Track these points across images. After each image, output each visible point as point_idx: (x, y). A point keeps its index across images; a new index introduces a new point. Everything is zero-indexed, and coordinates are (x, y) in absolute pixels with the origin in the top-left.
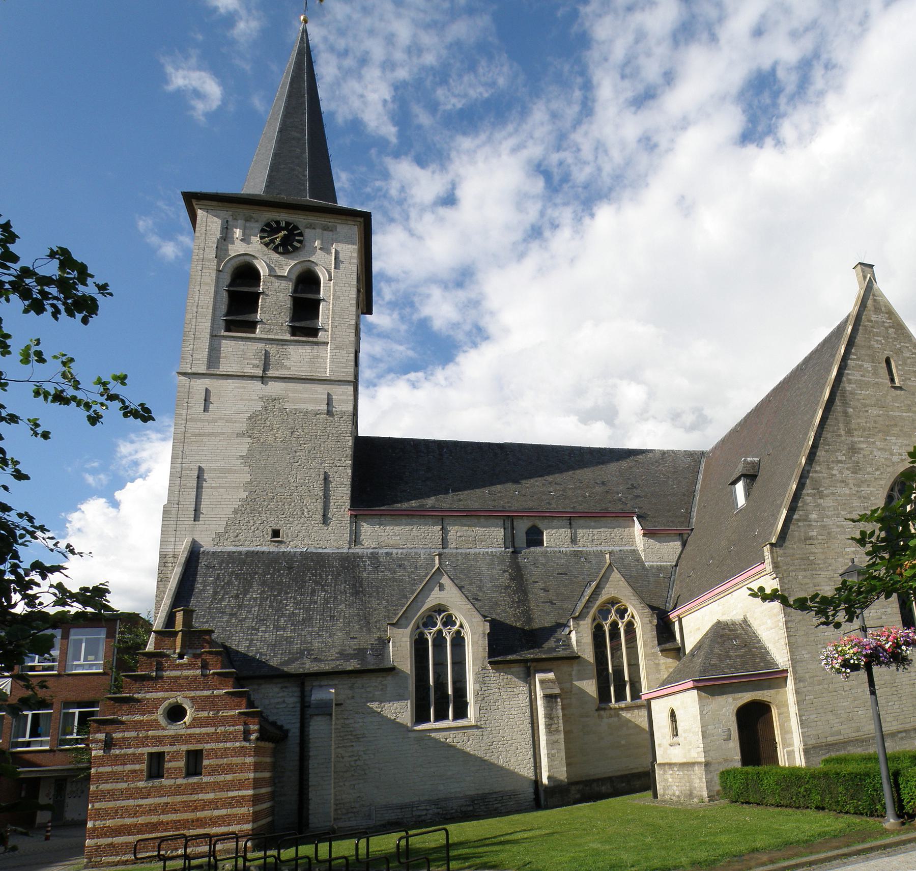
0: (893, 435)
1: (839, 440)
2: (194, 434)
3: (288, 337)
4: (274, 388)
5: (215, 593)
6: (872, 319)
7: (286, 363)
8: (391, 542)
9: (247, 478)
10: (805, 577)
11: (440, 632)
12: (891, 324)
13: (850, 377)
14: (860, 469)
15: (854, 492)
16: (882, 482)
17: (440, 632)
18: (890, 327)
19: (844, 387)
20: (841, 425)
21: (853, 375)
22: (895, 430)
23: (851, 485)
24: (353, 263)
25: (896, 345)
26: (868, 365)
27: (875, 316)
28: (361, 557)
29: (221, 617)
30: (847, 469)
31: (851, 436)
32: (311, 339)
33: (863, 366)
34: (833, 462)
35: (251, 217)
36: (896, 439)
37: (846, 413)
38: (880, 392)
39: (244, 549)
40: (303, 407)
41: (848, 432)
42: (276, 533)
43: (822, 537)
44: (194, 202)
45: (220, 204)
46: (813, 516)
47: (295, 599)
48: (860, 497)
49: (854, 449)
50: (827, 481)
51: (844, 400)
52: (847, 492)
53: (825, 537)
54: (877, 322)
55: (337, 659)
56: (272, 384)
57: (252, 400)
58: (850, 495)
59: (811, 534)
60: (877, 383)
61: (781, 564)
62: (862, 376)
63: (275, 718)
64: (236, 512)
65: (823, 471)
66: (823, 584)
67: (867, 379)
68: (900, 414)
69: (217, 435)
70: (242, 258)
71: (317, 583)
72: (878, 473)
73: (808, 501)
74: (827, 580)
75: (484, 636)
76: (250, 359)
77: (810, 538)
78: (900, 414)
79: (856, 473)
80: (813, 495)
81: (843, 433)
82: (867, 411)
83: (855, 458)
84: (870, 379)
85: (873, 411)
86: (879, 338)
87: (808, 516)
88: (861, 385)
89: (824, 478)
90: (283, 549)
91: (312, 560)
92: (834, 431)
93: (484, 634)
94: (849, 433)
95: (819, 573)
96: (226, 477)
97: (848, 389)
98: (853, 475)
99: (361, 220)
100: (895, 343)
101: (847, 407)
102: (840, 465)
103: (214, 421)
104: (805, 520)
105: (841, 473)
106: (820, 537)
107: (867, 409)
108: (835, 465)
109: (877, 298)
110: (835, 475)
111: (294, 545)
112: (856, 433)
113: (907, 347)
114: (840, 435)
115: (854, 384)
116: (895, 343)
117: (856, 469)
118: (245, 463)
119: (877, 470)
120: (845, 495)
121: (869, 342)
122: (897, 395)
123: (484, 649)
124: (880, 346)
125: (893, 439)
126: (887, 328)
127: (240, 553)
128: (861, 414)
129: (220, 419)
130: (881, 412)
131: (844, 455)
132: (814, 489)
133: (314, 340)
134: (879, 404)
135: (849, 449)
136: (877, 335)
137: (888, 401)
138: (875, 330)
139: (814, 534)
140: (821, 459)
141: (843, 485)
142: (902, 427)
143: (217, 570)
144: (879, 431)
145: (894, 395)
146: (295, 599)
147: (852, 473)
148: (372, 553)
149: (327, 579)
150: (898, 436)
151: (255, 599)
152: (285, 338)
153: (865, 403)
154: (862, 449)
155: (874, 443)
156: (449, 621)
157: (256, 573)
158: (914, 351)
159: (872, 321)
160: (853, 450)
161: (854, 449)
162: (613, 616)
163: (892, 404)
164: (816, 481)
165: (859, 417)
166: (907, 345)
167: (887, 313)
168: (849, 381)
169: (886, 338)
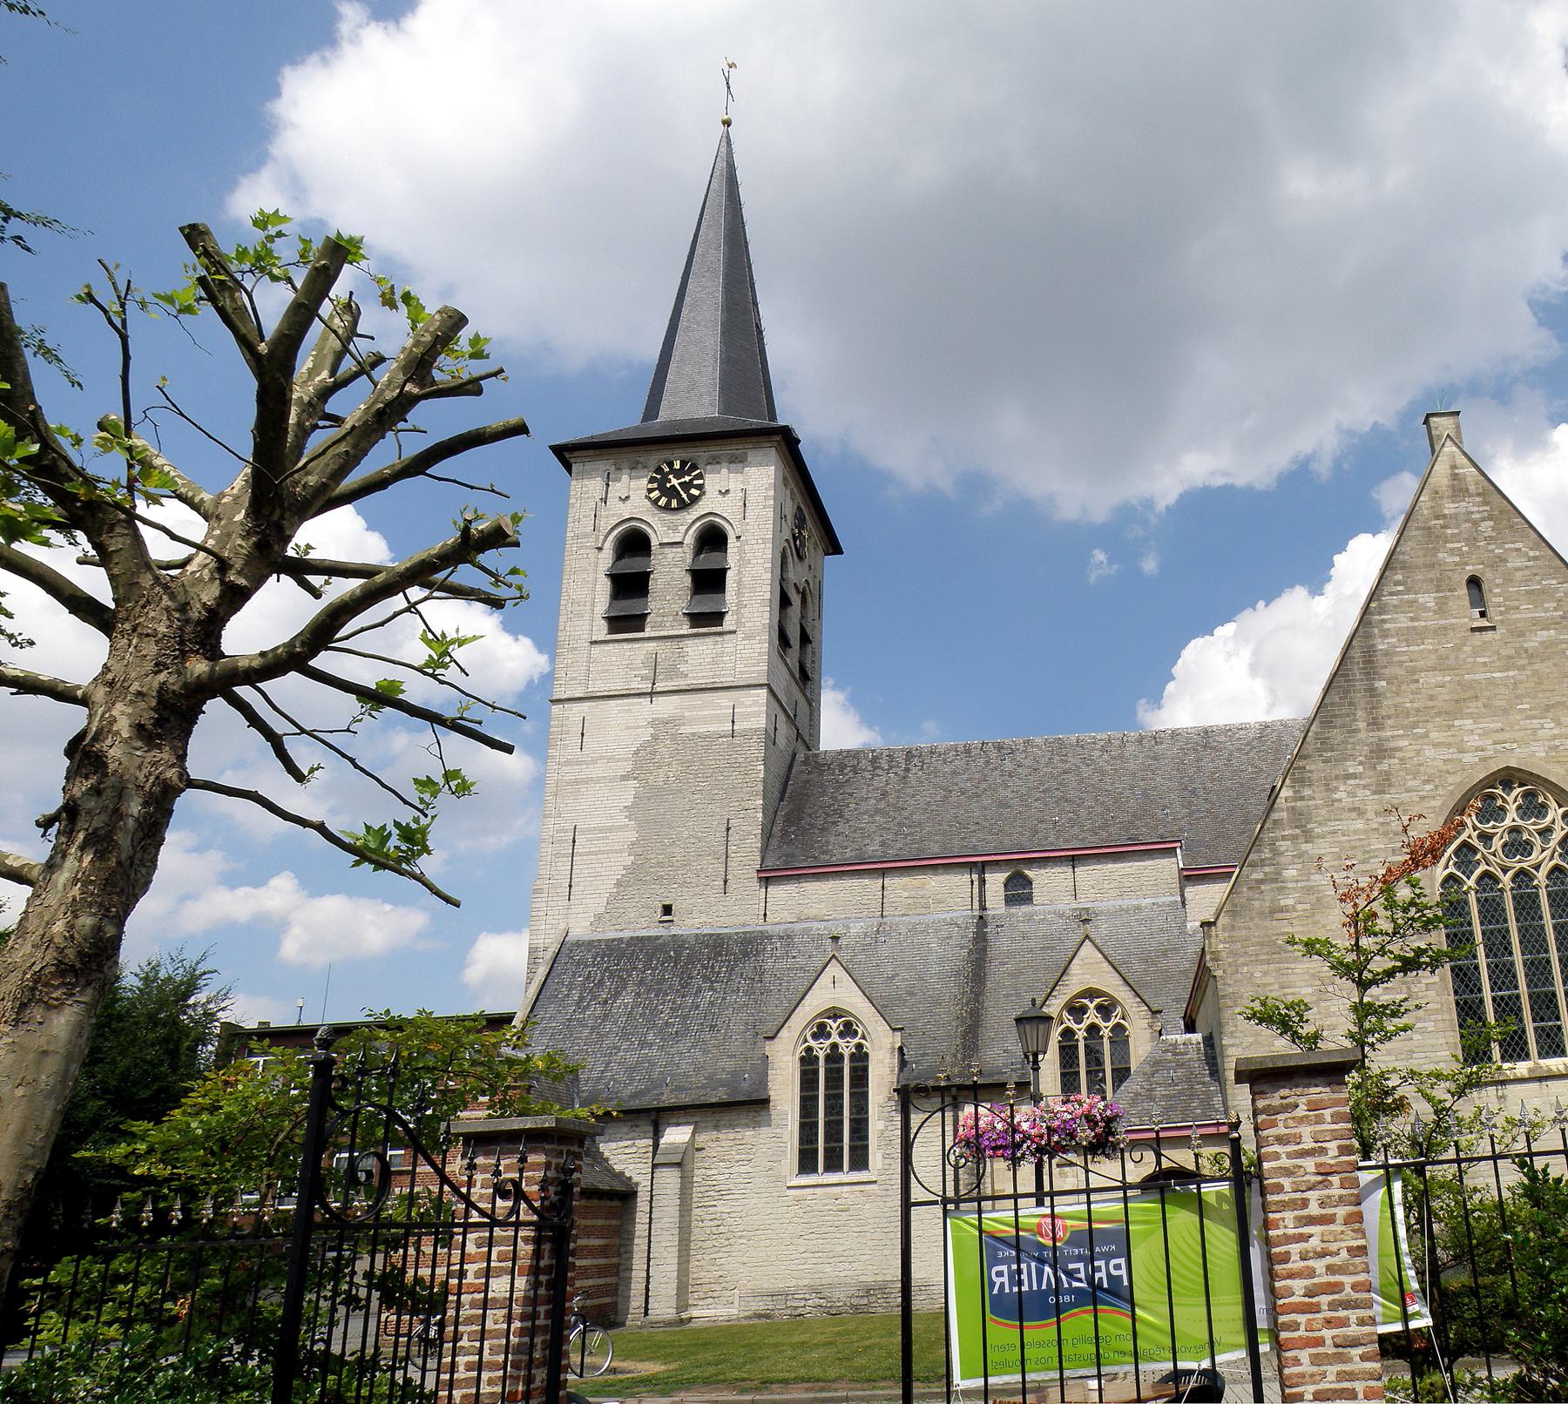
0: (1469, 715)
1: (1352, 740)
2: (569, 783)
3: (685, 629)
4: (666, 707)
5: (581, 999)
6: (1446, 512)
7: (683, 668)
8: (814, 912)
9: (633, 837)
10: (1265, 974)
11: (834, 1046)
12: (1486, 514)
13: (1387, 626)
14: (1390, 785)
15: (1375, 826)
16: (1437, 803)
17: (834, 1046)
18: (1484, 519)
19: (1374, 646)
20: (1360, 714)
21: (1393, 621)
22: (1473, 707)
23: (1370, 815)
24: (769, 506)
25: (1492, 551)
26: (1428, 599)
27: (1452, 505)
28: (770, 938)
29: (581, 1032)
30: (1365, 787)
31: (1378, 729)
32: (714, 629)
33: (1416, 601)
34: (1337, 778)
35: (638, 462)
36: (1475, 723)
37: (1371, 692)
38: (1448, 642)
39: (627, 934)
40: (702, 729)
41: (1373, 724)
42: (667, 910)
43: (1305, 906)
44: (567, 455)
45: (598, 452)
46: (1291, 873)
47: (674, 1003)
48: (1386, 834)
49: (1381, 751)
50: (1323, 812)
51: (1371, 668)
52: (1361, 826)
53: (1308, 907)
54: (1455, 516)
55: (703, 1087)
56: (660, 701)
57: (639, 727)
58: (1366, 832)
59: (1283, 903)
60: (1445, 628)
61: (1223, 954)
62: (1412, 619)
63: (623, 1167)
64: (618, 884)
65: (1316, 796)
66: (1298, 984)
67: (1423, 623)
68: (1489, 675)
69: (598, 780)
70: (627, 525)
71: (706, 978)
72: (1429, 787)
73: (1282, 849)
74: (1307, 977)
75: (892, 1052)
76: (638, 669)
77: (1282, 910)
78: (1489, 675)
79: (1383, 792)
80: (1294, 838)
81: (1362, 725)
82: (1417, 681)
83: (1384, 767)
84: (1430, 621)
85: (1428, 679)
86: (1459, 545)
87: (1279, 874)
88: (1410, 635)
89: (1317, 807)
90: (674, 931)
91: (707, 946)
92: (1343, 726)
93: (893, 1048)
94: (1375, 724)
95: (1292, 966)
96: (608, 838)
97: (1380, 647)
98: (1376, 797)
99: (778, 438)
100: (1491, 547)
101: (1374, 679)
102: (1351, 782)
103: (594, 761)
104: (1276, 881)
105: (1352, 794)
106: (1299, 907)
107: (1416, 677)
108: (1341, 782)
109: (1461, 471)
110: (1340, 800)
111: (689, 924)
112: (1390, 722)
113: (1517, 550)
114: (1357, 731)
115: (1393, 637)
116: (1491, 547)
117: (1383, 784)
118: (629, 817)
119: (1427, 782)
120: (1355, 832)
121: (1435, 555)
122: (1485, 643)
123: (893, 1071)
124: (1457, 559)
125: (1468, 723)
126: (1476, 523)
127: (621, 940)
128: (1404, 687)
129: (602, 758)
130: (1447, 679)
131: (1361, 763)
132: (1296, 827)
133: (718, 629)
134: (1441, 665)
135: (1371, 752)
136: (1455, 539)
137: (1462, 656)
138: (1449, 531)
139: (1290, 902)
140: (1315, 776)
141: (1354, 815)
142: (1489, 699)
143: (589, 966)
144: (1439, 714)
145: (1478, 643)
146: (674, 1003)
147: (1374, 793)
148: (785, 930)
149: (719, 973)
150: (1476, 717)
151: (626, 1005)
152: (681, 632)
153: (1415, 667)
154: (1400, 749)
155: (1426, 735)
156: (848, 1030)
157: (634, 969)
158: (1532, 554)
159: (1444, 516)
160: (1380, 751)
161: (1381, 751)
162: (1092, 1017)
163: (1470, 660)
164: (1300, 814)
165: (1398, 694)
166: (1518, 545)
167: (1479, 495)
168: (1385, 634)
169: (1472, 541)
